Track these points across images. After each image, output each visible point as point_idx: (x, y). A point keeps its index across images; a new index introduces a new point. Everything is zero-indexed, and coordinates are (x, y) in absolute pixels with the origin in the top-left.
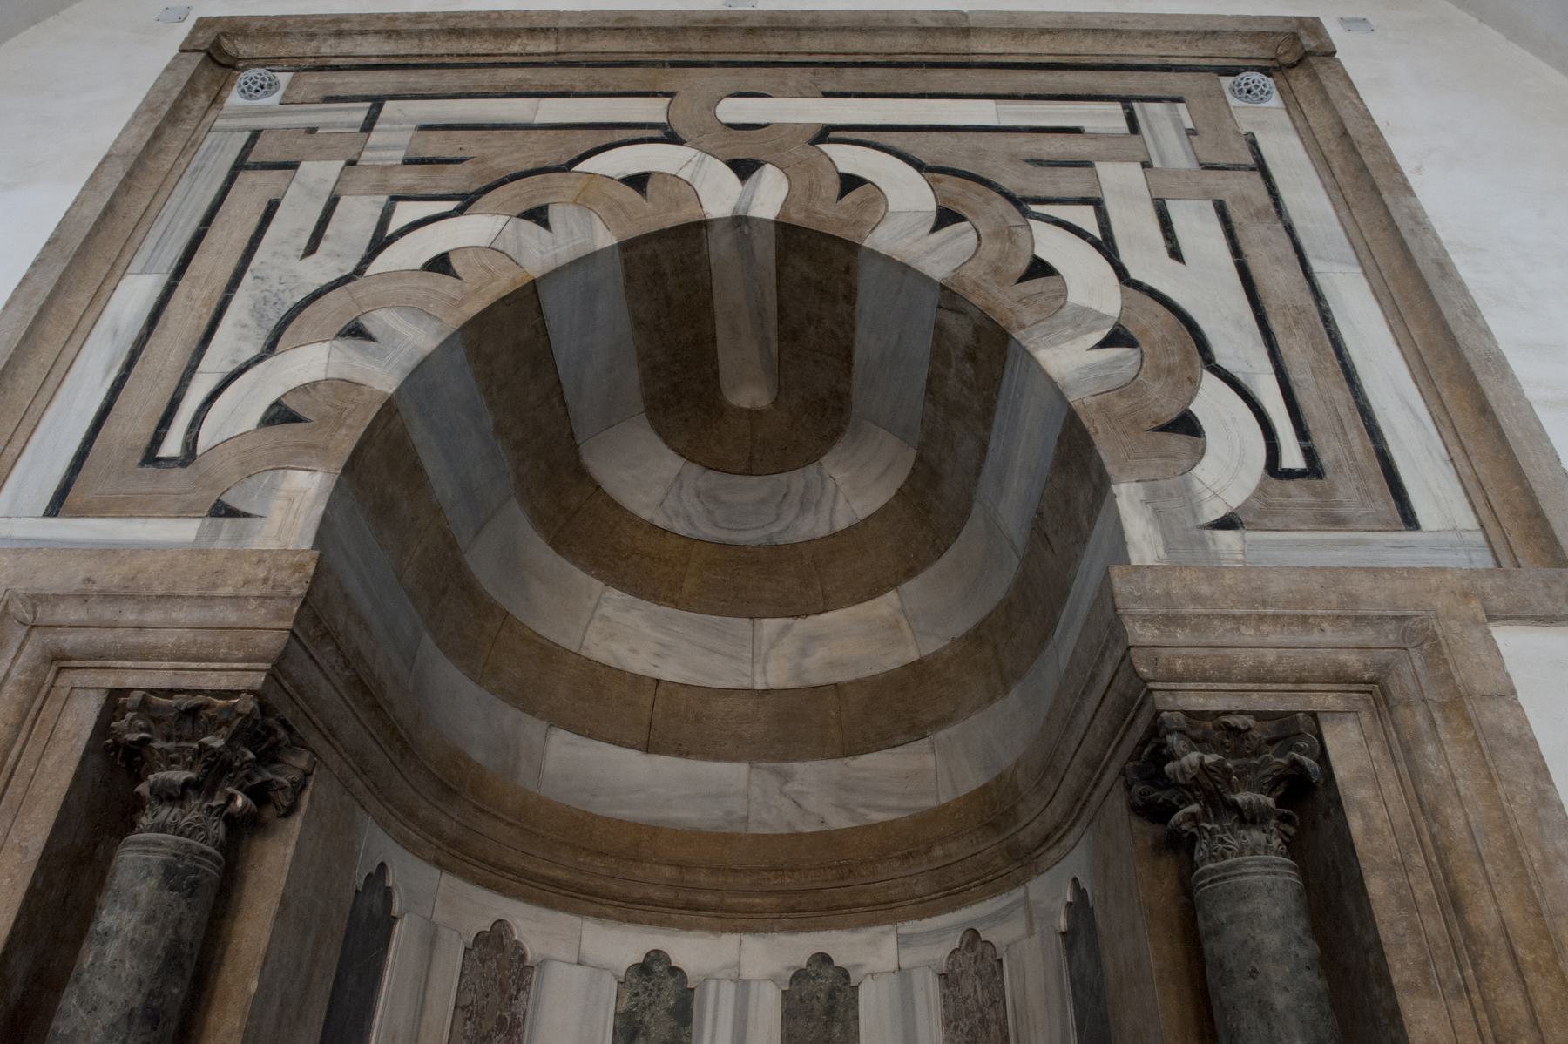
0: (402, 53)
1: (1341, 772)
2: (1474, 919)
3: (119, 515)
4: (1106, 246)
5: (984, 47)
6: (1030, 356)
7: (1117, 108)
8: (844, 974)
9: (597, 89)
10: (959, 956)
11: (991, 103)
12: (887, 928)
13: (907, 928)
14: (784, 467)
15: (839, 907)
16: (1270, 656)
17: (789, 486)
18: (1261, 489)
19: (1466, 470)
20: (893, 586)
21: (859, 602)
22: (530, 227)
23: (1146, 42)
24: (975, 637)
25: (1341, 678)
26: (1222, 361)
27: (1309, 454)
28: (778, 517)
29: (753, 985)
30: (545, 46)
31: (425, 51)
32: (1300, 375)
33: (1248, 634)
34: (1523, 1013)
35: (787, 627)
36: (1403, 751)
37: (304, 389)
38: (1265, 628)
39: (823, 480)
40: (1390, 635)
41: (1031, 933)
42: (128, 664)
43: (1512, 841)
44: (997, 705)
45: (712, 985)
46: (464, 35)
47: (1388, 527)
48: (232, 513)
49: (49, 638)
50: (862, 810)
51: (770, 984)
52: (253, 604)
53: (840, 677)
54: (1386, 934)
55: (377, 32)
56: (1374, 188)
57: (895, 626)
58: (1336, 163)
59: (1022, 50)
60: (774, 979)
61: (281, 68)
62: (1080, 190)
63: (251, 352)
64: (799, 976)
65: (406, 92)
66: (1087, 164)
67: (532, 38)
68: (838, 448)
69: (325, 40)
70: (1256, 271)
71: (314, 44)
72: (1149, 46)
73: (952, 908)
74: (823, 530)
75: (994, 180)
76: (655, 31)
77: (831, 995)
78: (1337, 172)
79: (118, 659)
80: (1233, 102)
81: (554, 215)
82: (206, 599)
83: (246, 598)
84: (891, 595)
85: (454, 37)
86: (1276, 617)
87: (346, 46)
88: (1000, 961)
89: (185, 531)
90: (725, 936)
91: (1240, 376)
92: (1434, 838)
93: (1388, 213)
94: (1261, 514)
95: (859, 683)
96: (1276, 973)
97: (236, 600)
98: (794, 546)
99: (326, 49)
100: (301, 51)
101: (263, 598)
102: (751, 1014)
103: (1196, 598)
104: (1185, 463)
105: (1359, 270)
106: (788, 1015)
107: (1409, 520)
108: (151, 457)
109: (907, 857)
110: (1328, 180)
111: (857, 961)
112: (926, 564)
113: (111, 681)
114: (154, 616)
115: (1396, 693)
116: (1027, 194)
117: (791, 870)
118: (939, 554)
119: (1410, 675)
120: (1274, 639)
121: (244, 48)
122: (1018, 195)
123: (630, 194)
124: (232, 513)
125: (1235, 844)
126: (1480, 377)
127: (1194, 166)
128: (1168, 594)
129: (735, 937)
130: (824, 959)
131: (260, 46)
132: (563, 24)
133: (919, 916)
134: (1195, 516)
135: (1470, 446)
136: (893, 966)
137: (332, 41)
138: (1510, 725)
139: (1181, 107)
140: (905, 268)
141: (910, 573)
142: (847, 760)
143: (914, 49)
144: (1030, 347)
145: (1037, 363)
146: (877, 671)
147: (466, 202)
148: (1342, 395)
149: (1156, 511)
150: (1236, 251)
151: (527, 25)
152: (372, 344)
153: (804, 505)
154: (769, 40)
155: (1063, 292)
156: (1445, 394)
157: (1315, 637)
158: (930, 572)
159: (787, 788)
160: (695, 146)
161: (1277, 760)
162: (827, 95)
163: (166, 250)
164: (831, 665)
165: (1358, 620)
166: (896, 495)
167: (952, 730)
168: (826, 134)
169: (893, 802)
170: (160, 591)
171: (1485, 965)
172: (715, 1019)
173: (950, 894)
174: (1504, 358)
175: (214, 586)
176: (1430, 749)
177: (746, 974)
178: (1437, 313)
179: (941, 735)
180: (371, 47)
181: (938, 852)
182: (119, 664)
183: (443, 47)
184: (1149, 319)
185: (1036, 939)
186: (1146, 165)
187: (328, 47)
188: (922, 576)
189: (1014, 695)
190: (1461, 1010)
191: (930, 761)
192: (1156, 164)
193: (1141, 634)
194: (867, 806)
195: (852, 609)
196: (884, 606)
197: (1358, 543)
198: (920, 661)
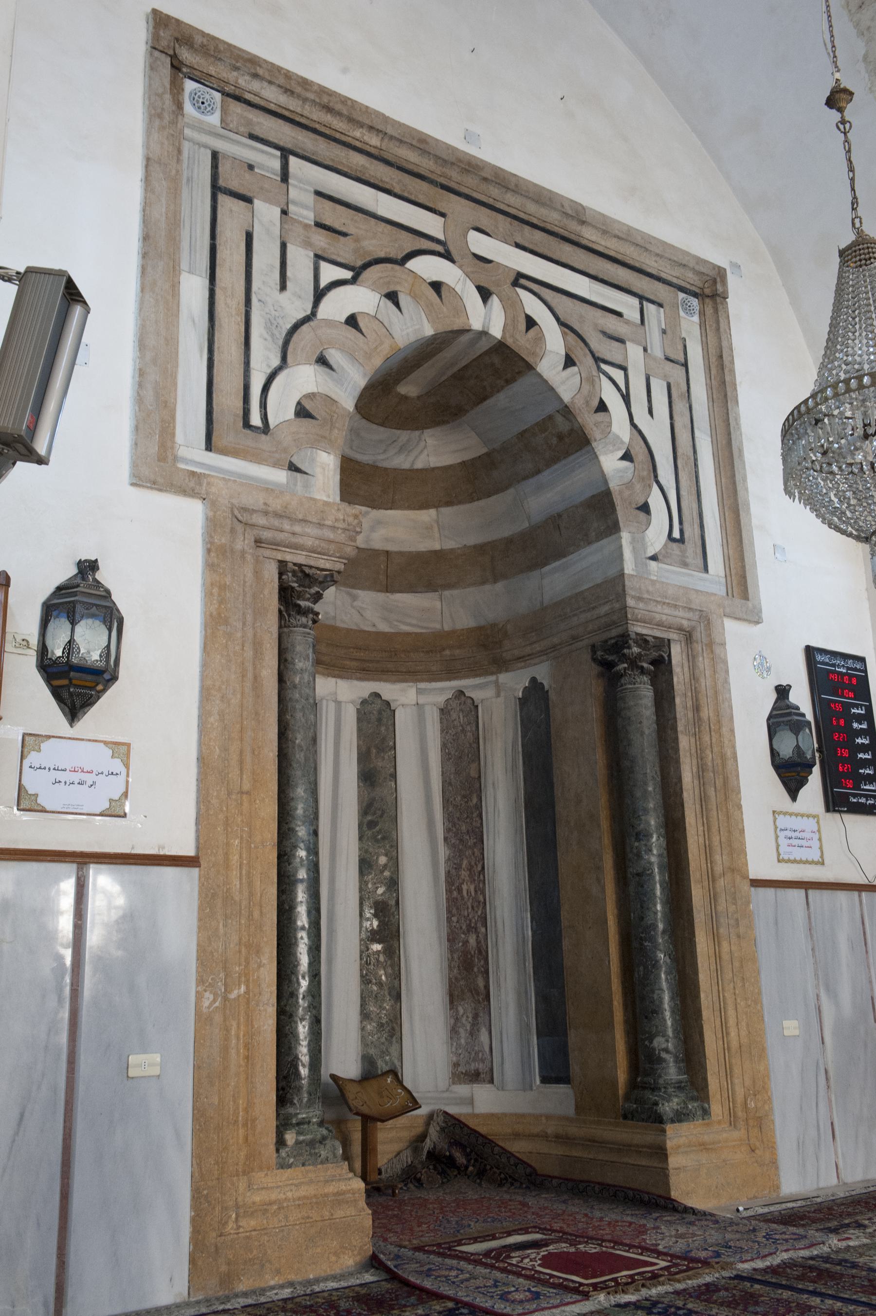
0: (291, 108)
1: (674, 662)
2: (702, 714)
3: (245, 458)
4: (626, 399)
5: (589, 235)
6: (597, 457)
7: (635, 302)
8: (388, 703)
9: (406, 194)
10: (451, 701)
11: (586, 280)
12: (411, 684)
13: (422, 685)
14: (401, 426)
15: (388, 671)
16: (664, 618)
17: (398, 438)
18: (665, 545)
19: (726, 551)
20: (436, 506)
21: (414, 509)
22: (390, 304)
23: (654, 259)
24: (480, 549)
25: (680, 629)
26: (660, 479)
27: (682, 532)
28: (385, 451)
29: (343, 705)
30: (374, 141)
31: (305, 113)
32: (683, 493)
33: (659, 608)
34: (709, 742)
35: (367, 513)
36: (692, 658)
37: (311, 396)
38: (665, 607)
39: (420, 440)
40: (695, 616)
41: (498, 695)
42: (288, 550)
43: (716, 692)
44: (487, 587)
45: (324, 702)
46: (331, 112)
47: (226, 156)
48: (297, 470)
49: (255, 532)
50: (396, 623)
51: (351, 705)
52: (340, 531)
53: (390, 547)
54: (678, 716)
55: (279, 86)
56: (726, 396)
57: (429, 528)
58: (714, 372)
59: (603, 243)
60: (352, 702)
61: (211, 85)
62: (618, 359)
63: (276, 362)
64: (364, 702)
65: (299, 151)
66: (621, 341)
67: (369, 132)
68: (439, 429)
69: (243, 75)
70: (677, 430)
71: (235, 74)
72: (656, 261)
73: (449, 679)
74: (406, 466)
75: (588, 341)
76: (437, 158)
77: (380, 712)
78: (713, 377)
79: (284, 547)
80: (682, 313)
81: (403, 299)
82: (320, 525)
83: (338, 528)
84: (432, 512)
85: (325, 110)
86: (669, 604)
87: (255, 85)
88: (477, 706)
89: (280, 476)
90: (330, 679)
91: (665, 488)
92: (695, 688)
93: (728, 414)
94: (664, 557)
95: (401, 554)
96: (645, 723)
97: (333, 528)
98: (386, 469)
99: (242, 82)
100: (225, 75)
101: (345, 530)
102: (343, 718)
103: (648, 592)
104: (644, 527)
105: (710, 439)
106: (359, 720)
107: (706, 569)
108: (247, 424)
109: (428, 652)
110: (708, 381)
111: (394, 698)
112: (460, 503)
113: (280, 557)
114: (297, 529)
115: (694, 638)
116: (601, 356)
117: (365, 650)
118: (472, 500)
119: (699, 634)
120: (666, 611)
121: (186, 55)
122: (597, 355)
123: (431, 293)
124: (297, 470)
125: (639, 680)
126: (741, 513)
127: (663, 357)
128: (640, 589)
129: (334, 680)
130: (377, 695)
131: (197, 58)
132: (390, 131)
133: (430, 680)
134: (645, 553)
135: (729, 540)
136: (414, 702)
137: (247, 78)
138: (722, 655)
139: (662, 310)
140: (552, 389)
141: (449, 504)
142: (388, 594)
143: (556, 223)
144: (598, 453)
145: (599, 462)
146: (413, 549)
147: (357, 273)
148: (695, 506)
149: (634, 548)
150: (671, 417)
151: (370, 124)
152: (333, 373)
153: (401, 450)
154: (491, 188)
155: (610, 424)
156: (727, 514)
157: (676, 613)
158: (462, 507)
159: (355, 604)
160: (460, 267)
161: (655, 654)
162: (518, 246)
163: (198, 255)
164: (387, 540)
165: (690, 609)
166: (461, 463)
167: (455, 592)
168: (519, 279)
169: (414, 622)
170: (300, 517)
171: (702, 728)
172: (327, 718)
173: (450, 673)
174: (749, 504)
175: (323, 519)
176: (701, 659)
177: (340, 698)
178: (733, 476)
179: (447, 593)
180: (272, 95)
181: (447, 652)
182: (284, 549)
183: (317, 115)
184: (639, 451)
185: (501, 700)
186: (645, 350)
187: (244, 82)
188: (455, 508)
189: (500, 586)
190: (693, 740)
191: (438, 604)
192: (649, 351)
193: (630, 602)
194: (397, 621)
195: (406, 512)
196: (428, 516)
197: (689, 575)
198: (441, 551)
